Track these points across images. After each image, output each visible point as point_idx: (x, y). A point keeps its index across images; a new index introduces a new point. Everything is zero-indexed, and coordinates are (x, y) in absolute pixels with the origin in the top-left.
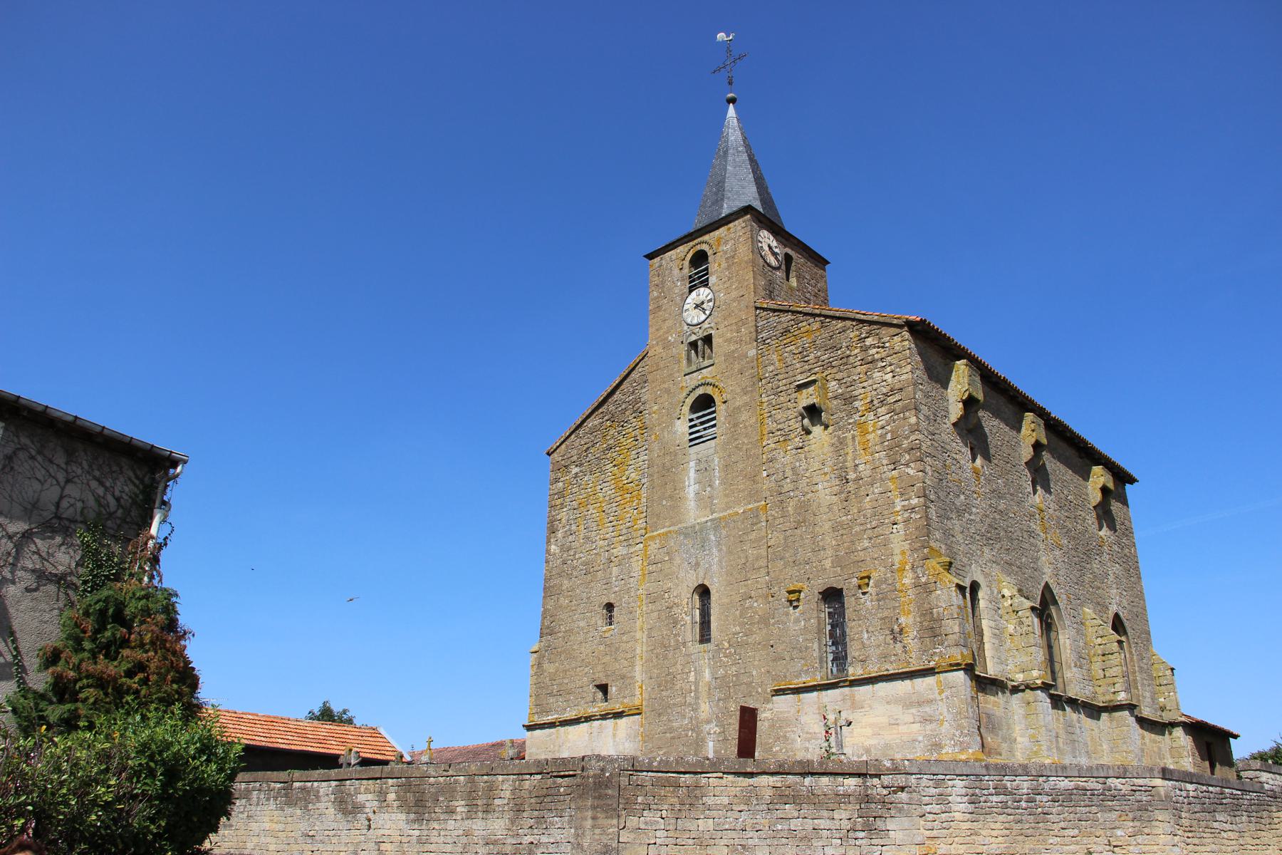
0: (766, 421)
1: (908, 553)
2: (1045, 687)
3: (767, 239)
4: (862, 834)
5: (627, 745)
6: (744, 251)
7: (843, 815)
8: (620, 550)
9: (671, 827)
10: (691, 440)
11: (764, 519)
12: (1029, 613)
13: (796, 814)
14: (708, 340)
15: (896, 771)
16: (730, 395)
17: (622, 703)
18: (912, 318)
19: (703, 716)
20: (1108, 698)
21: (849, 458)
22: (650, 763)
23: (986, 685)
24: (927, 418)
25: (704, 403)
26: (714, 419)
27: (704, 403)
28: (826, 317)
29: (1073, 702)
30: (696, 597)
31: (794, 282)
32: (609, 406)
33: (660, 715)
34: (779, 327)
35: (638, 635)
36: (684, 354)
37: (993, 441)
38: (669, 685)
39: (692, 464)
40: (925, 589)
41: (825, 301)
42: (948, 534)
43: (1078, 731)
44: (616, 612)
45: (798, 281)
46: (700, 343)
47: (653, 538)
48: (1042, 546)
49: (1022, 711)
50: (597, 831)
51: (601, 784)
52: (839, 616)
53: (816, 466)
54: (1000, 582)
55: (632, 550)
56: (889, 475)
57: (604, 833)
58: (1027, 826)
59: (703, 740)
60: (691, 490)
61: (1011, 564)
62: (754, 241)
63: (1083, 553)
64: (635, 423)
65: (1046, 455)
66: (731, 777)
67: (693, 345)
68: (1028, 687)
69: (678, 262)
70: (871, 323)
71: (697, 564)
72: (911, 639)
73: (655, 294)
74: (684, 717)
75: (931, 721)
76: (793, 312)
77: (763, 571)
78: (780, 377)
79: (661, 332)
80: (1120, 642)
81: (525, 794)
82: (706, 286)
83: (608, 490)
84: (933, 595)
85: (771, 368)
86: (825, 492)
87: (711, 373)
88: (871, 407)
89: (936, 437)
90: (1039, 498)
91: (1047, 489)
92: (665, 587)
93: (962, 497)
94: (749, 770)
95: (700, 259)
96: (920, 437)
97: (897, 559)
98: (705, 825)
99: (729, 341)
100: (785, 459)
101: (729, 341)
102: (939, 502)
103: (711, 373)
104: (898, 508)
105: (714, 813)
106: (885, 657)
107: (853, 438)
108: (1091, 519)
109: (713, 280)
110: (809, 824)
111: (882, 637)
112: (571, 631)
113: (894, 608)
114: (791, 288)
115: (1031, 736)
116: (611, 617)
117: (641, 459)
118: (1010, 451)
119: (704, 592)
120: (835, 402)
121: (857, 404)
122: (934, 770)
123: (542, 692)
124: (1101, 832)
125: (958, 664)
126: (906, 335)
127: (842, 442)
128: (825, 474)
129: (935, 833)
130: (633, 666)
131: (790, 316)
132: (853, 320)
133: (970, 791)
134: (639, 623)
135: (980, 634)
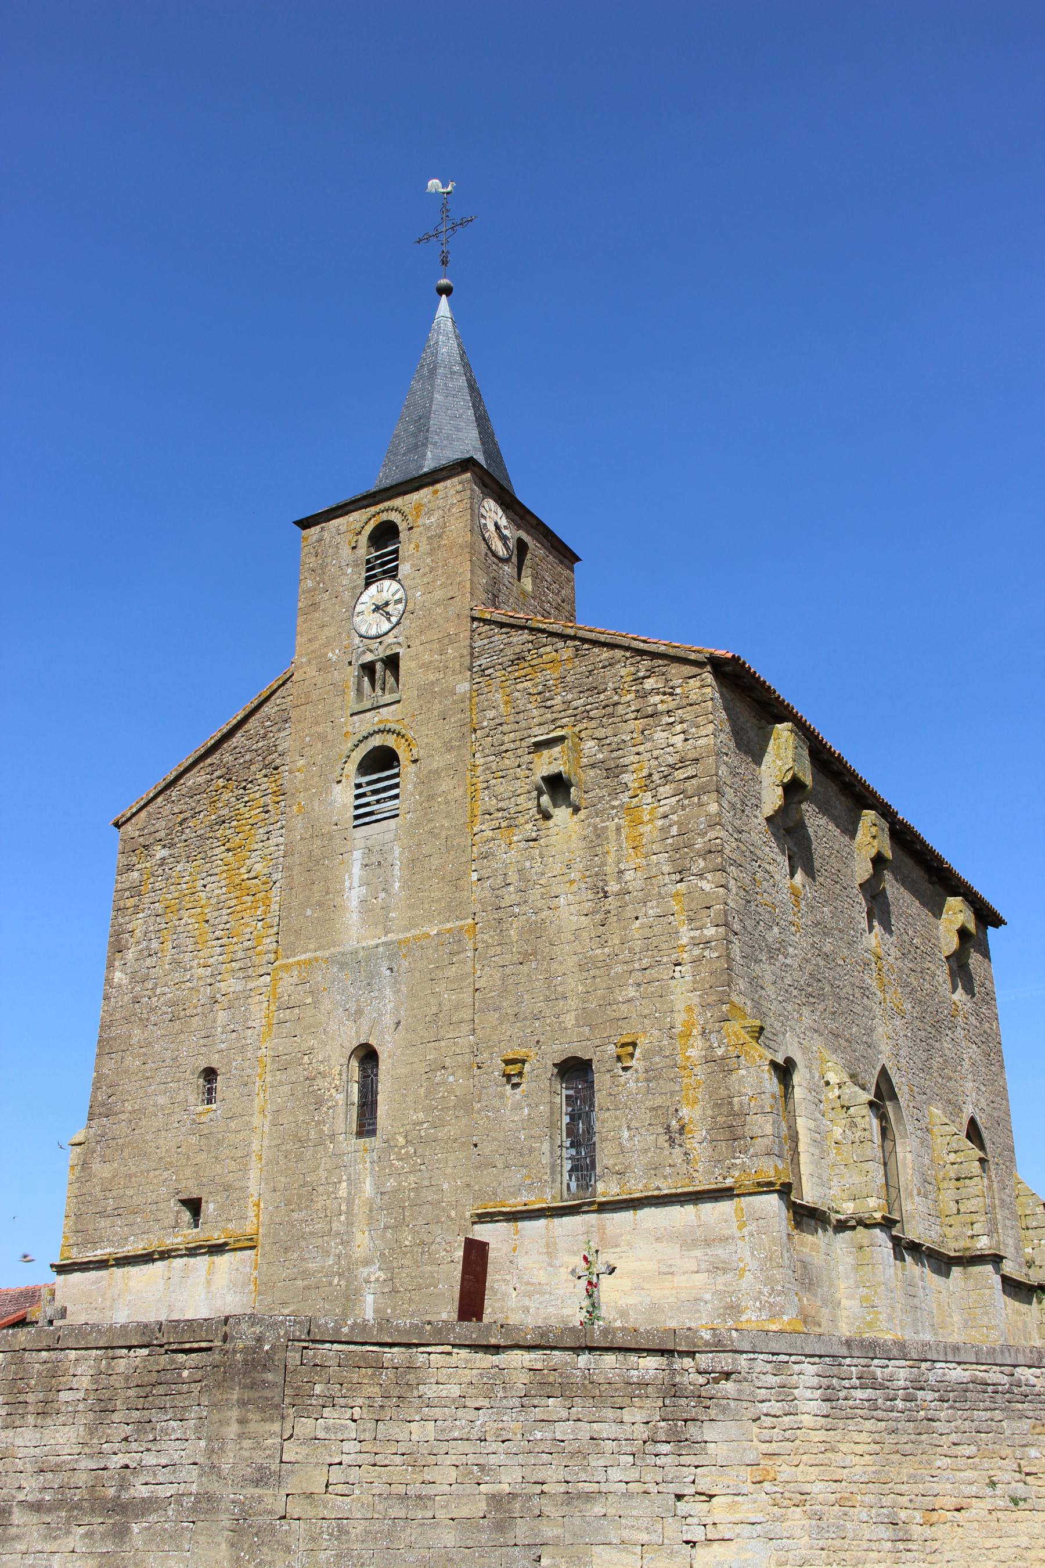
0: (480, 795)
1: (698, 1010)
2: (887, 1224)
3: (493, 513)
4: (665, 1448)
5: (229, 1298)
6: (458, 530)
7: (637, 1417)
8: (231, 985)
9: (367, 1436)
10: (357, 817)
11: (470, 945)
12: (866, 1111)
13: (564, 1414)
14: (392, 662)
15: (718, 1347)
16: (424, 750)
17: (224, 1230)
18: (720, 652)
19: (359, 1253)
20: (963, 1244)
21: (610, 860)
22: (337, 1329)
23: (807, 1217)
24: (733, 806)
25: (381, 760)
26: (397, 786)
27: (381, 760)
28: (584, 641)
29: (914, 1248)
30: (355, 1063)
31: (527, 584)
32: (225, 756)
33: (286, 1250)
34: (509, 651)
35: (257, 1120)
36: (352, 681)
37: (819, 849)
38: (304, 1203)
39: (357, 854)
40: (722, 1066)
41: (571, 617)
42: (756, 984)
43: (921, 1293)
44: (220, 1082)
45: (534, 583)
46: (379, 666)
47: (286, 968)
48: (878, 1011)
49: (850, 1260)
50: (247, 1443)
51: (257, 1362)
52: (583, 1101)
53: (558, 868)
54: (824, 1061)
55: (251, 985)
56: (673, 889)
57: (258, 1447)
58: (905, 1438)
59: (358, 1292)
60: (354, 895)
61: (837, 1036)
62: (476, 515)
63: (932, 1026)
64: (265, 784)
65: (888, 875)
66: (464, 1353)
67: (368, 669)
68: (861, 1223)
69: (350, 536)
70: (654, 655)
71: (359, 1012)
72: (697, 1142)
73: (310, 583)
74: (327, 1253)
75: (725, 1271)
76: (532, 630)
77: (466, 1028)
78: (505, 728)
79: (316, 645)
80: (982, 1161)
81: (117, 1382)
82: (393, 577)
83: (217, 889)
84: (734, 1077)
85: (491, 714)
86: (570, 911)
87: (395, 715)
88: (648, 783)
89: (744, 835)
90: (875, 939)
91: (887, 927)
92: (304, 1047)
93: (776, 930)
94: (493, 1341)
95: (385, 534)
96: (722, 834)
97: (680, 1018)
98: (421, 1431)
99: (426, 666)
100: (509, 855)
101: (426, 666)
102: (744, 931)
103: (395, 715)
104: (684, 941)
105: (437, 1412)
106: (655, 1168)
107: (618, 829)
108: (943, 974)
109: (405, 569)
110: (585, 1430)
111: (652, 1138)
112: (143, 1110)
113: (672, 1093)
114: (524, 593)
115: (864, 1299)
116: (210, 1091)
117: (273, 841)
118: (841, 866)
119: (368, 1056)
120: (592, 773)
121: (626, 778)
122: (775, 1347)
123: (86, 1210)
124: (1008, 1451)
125: (770, 1184)
126: (709, 678)
127: (600, 834)
128: (572, 882)
129: (773, 1447)
130: (245, 1169)
131: (526, 636)
132: (627, 648)
133: (825, 1382)
134: (257, 1102)
135: (794, 1138)
